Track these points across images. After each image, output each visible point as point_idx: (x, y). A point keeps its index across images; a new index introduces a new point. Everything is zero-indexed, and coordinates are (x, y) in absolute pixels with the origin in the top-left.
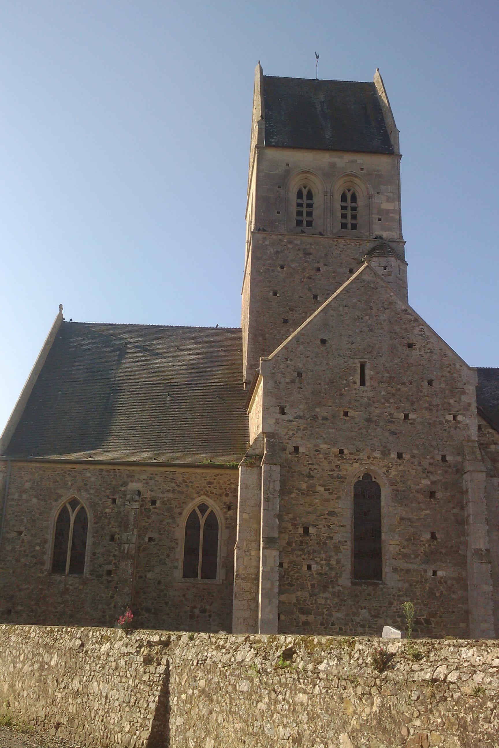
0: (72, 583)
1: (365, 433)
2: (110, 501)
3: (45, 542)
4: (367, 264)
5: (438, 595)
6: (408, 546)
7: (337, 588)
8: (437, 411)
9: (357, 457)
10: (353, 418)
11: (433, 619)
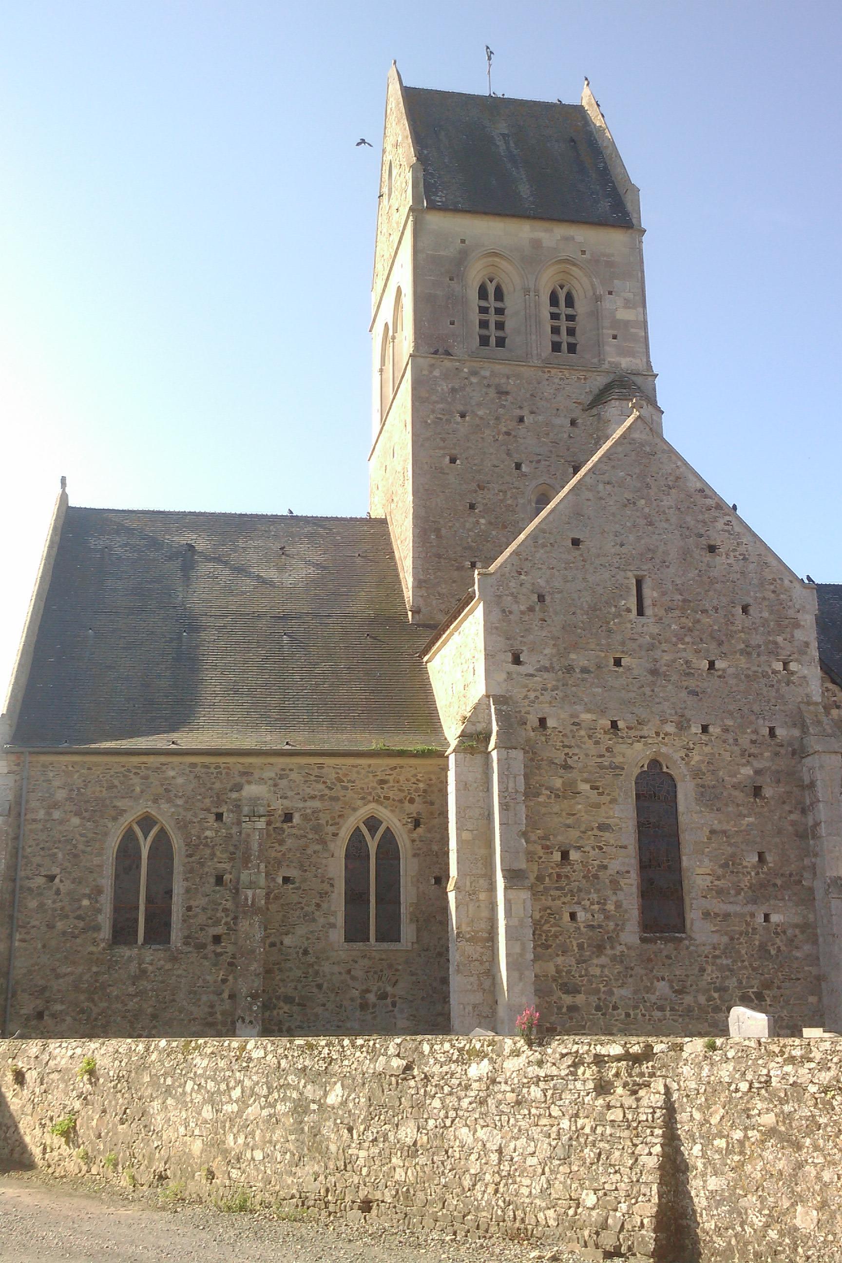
0: (153, 960)
1: (649, 693)
2: (212, 818)
3: (99, 891)
4: (638, 413)
5: (773, 952)
6: (724, 876)
7: (619, 948)
8: (759, 655)
9: (639, 733)
10: (629, 669)
11: (767, 992)
